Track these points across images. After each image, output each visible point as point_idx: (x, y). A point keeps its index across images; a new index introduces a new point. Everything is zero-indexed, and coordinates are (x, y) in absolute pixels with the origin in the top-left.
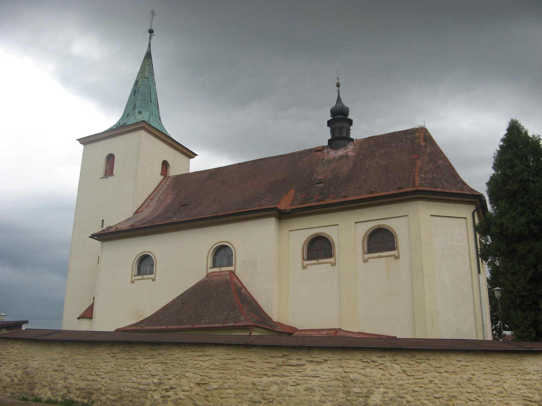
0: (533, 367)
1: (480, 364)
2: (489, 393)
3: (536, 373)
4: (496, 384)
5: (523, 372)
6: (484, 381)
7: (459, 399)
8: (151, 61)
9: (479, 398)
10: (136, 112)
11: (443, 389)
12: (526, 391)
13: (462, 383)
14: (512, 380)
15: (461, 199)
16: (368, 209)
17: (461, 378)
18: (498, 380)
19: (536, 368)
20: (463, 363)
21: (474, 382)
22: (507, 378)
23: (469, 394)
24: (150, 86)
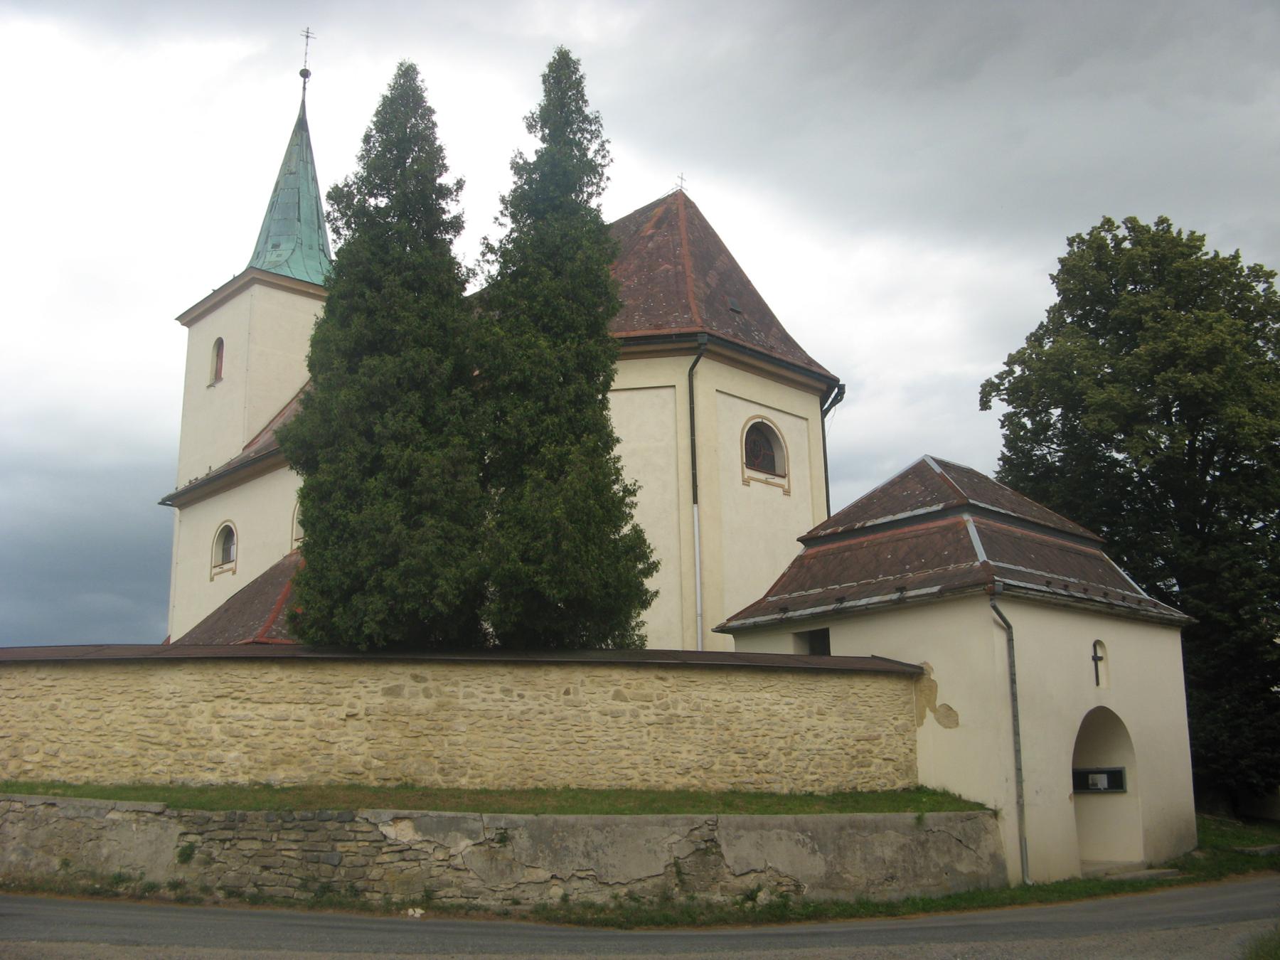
0: (168, 686)
1: (72, 682)
2: (251, 736)
3: (172, 696)
4: (94, 715)
5: (147, 695)
6: (75, 711)
7: (33, 740)
8: (304, 137)
9: (62, 738)
10: (269, 246)
11: (12, 723)
12: (147, 725)
13: (40, 714)
14: (122, 708)
15: (670, 346)
16: (755, 378)
17: (40, 706)
18: (96, 709)
19: (171, 688)
20: (48, 682)
21: (58, 712)
22: (114, 704)
23: (48, 731)
24: (299, 189)
